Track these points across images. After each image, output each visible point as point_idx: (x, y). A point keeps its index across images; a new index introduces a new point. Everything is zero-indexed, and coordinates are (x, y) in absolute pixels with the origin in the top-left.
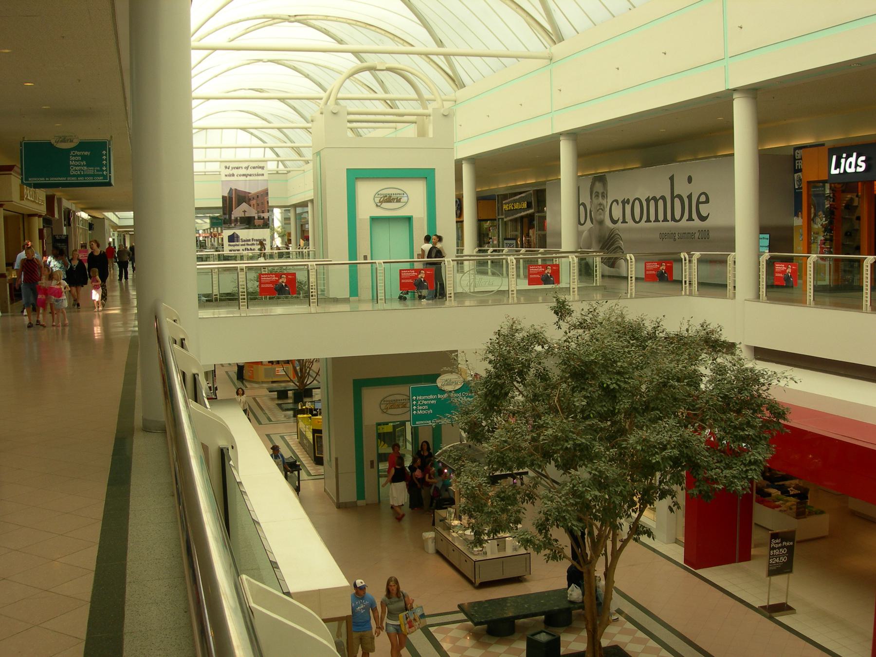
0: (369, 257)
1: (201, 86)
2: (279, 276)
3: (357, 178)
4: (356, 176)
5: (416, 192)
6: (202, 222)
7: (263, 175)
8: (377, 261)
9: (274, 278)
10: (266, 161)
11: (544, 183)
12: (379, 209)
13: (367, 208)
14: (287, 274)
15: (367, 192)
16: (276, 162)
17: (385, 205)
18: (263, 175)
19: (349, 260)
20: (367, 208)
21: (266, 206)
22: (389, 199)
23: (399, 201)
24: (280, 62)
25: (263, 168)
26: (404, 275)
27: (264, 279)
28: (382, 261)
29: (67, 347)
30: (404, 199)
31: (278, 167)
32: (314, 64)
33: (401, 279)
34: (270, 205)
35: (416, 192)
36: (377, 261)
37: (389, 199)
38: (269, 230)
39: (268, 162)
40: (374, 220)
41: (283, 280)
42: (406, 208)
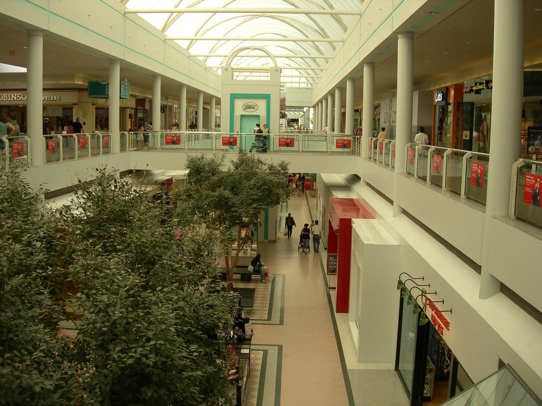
0: (239, 132)
1: (233, 29)
2: (287, 139)
3: (234, 98)
4: (234, 97)
5: (262, 104)
6: (299, 114)
7: (283, 90)
8: (271, 134)
9: (171, 138)
10: (285, 83)
11: (380, 103)
12: (245, 111)
13: (239, 110)
14: (234, 138)
15: (239, 104)
16: (306, 84)
17: (247, 110)
18: (283, 90)
19: (230, 132)
20: (239, 110)
21: (284, 106)
22: (249, 107)
23: (254, 108)
24: (274, 17)
25: (283, 86)
26: (281, 140)
27: (281, 140)
28: (273, 134)
29: (220, 168)
30: (256, 108)
31: (307, 86)
32: (292, 19)
33: (280, 142)
34: (286, 105)
35: (262, 104)
36: (243, 134)
37: (249, 107)
38: (285, 119)
39: (286, 84)
40: (242, 116)
41: (289, 141)
42: (257, 111)
